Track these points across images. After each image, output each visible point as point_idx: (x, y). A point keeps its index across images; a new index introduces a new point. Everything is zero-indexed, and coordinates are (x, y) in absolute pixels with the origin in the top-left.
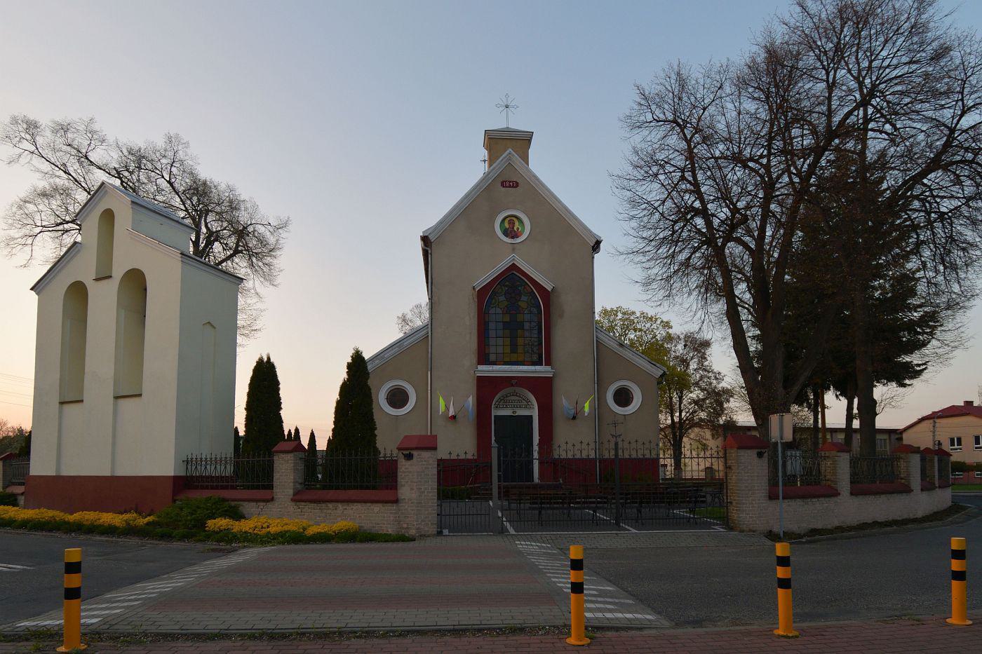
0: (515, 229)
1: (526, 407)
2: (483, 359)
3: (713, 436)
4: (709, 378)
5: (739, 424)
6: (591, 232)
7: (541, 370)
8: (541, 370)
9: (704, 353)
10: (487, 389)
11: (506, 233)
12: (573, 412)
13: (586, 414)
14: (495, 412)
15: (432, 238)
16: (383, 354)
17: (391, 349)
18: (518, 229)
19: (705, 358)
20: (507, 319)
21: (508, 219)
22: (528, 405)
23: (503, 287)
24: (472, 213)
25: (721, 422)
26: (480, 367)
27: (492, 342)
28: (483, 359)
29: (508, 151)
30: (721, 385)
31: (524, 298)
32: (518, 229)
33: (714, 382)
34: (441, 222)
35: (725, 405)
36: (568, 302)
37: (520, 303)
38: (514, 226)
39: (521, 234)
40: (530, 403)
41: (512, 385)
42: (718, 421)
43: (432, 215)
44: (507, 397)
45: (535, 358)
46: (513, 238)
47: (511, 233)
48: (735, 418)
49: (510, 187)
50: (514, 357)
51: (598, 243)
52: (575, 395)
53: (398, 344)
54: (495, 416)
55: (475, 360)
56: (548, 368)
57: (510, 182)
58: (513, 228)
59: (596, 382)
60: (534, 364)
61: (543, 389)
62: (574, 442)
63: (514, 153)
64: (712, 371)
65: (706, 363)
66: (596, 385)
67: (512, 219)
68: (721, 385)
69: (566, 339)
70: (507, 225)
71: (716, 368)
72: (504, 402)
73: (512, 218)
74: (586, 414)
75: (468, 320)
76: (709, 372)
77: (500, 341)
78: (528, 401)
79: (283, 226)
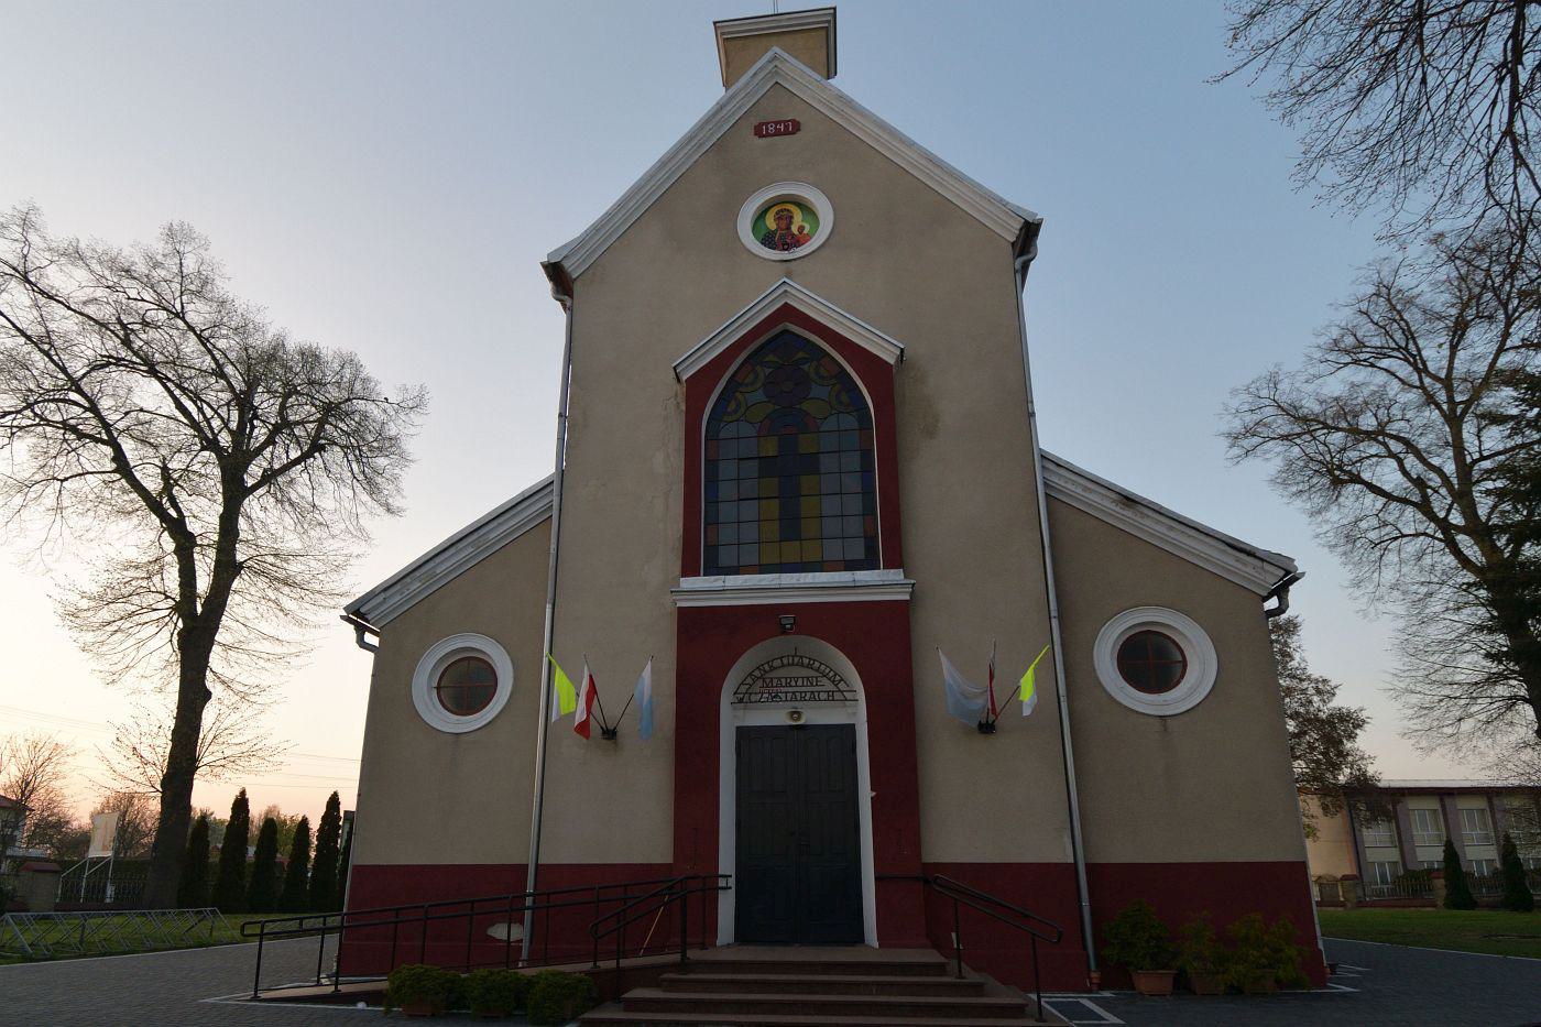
0: (794, 229)
1: (831, 697)
2: (698, 555)
3: (1325, 808)
4: (1303, 691)
5: (1380, 785)
6: (1005, 204)
7: (878, 583)
8: (878, 583)
9: (1286, 644)
10: (707, 640)
11: (768, 240)
12: (981, 702)
13: (1027, 712)
14: (730, 719)
15: (573, 268)
16: (431, 564)
17: (452, 550)
18: (801, 229)
19: (1290, 656)
20: (770, 448)
21: (775, 209)
22: (837, 695)
23: (759, 369)
24: (677, 203)
25: (1342, 779)
26: (688, 583)
27: (727, 511)
28: (698, 555)
29: (769, 55)
30: (1331, 705)
31: (817, 391)
32: (801, 229)
33: (1316, 699)
34: (596, 229)
35: (1348, 745)
36: (949, 392)
37: (805, 406)
38: (791, 223)
39: (808, 238)
40: (842, 686)
41: (784, 632)
42: (1335, 778)
43: (573, 212)
44: (773, 669)
45: (857, 551)
46: (786, 247)
47: (781, 239)
48: (1371, 770)
49: (778, 133)
50: (791, 551)
51: (1030, 230)
52: (984, 646)
53: (470, 539)
54: (743, 734)
55: (677, 569)
56: (896, 575)
57: (777, 123)
58: (789, 228)
59: (1054, 613)
60: (851, 566)
61: (883, 642)
62: (989, 814)
63: (786, 56)
64: (1308, 678)
65: (1294, 664)
66: (1055, 623)
67: (784, 207)
68: (1331, 705)
69: (944, 491)
70: (771, 223)
71: (1315, 671)
72: (762, 685)
73: (789, 207)
74: (1027, 712)
75: (665, 461)
76: (1301, 680)
77: (750, 510)
78: (837, 679)
79: (417, 404)
